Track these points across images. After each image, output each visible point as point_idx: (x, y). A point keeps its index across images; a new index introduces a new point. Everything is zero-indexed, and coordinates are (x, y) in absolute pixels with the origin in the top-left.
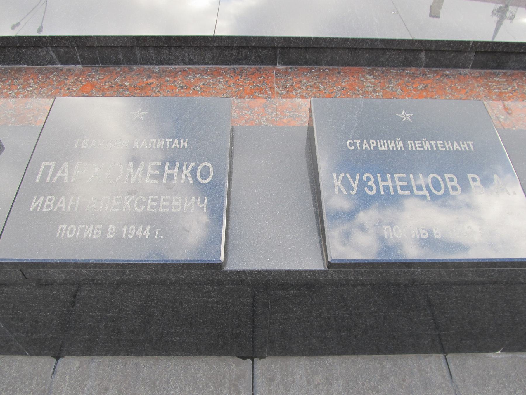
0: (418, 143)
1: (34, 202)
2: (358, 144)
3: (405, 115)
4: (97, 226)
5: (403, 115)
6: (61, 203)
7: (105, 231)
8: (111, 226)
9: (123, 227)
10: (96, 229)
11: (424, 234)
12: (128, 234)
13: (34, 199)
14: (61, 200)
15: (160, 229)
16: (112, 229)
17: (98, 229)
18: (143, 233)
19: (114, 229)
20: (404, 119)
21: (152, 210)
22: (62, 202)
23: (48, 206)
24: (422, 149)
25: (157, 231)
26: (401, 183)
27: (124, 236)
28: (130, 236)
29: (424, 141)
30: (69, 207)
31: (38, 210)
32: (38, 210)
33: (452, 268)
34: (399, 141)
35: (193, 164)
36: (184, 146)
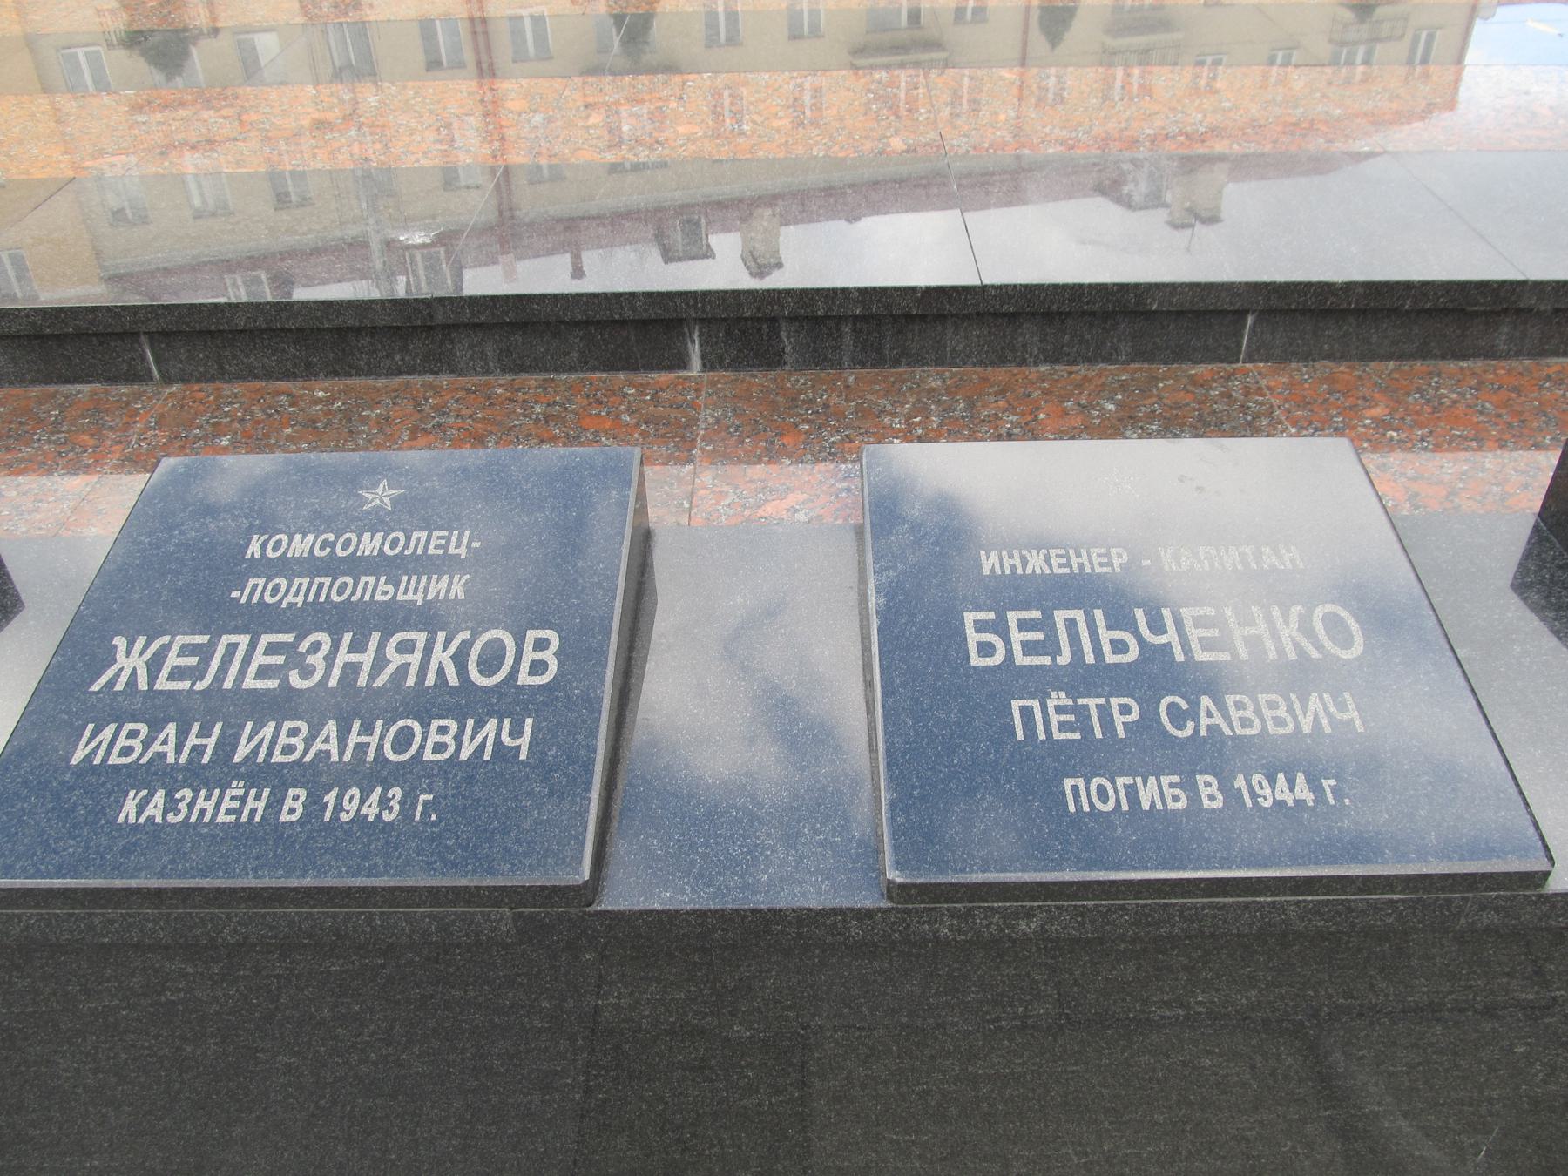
3: (382, 501)
6: (1210, 715)
7: (275, 804)
8: (292, 792)
9: (327, 792)
11: (1176, 799)
12: (338, 808)
13: (87, 734)
19: (303, 798)
20: (381, 487)
22: (328, 738)
23: (289, 749)
24: (1067, 571)
26: (1062, 718)
27: (328, 816)
33: (993, 902)
35: (466, 635)
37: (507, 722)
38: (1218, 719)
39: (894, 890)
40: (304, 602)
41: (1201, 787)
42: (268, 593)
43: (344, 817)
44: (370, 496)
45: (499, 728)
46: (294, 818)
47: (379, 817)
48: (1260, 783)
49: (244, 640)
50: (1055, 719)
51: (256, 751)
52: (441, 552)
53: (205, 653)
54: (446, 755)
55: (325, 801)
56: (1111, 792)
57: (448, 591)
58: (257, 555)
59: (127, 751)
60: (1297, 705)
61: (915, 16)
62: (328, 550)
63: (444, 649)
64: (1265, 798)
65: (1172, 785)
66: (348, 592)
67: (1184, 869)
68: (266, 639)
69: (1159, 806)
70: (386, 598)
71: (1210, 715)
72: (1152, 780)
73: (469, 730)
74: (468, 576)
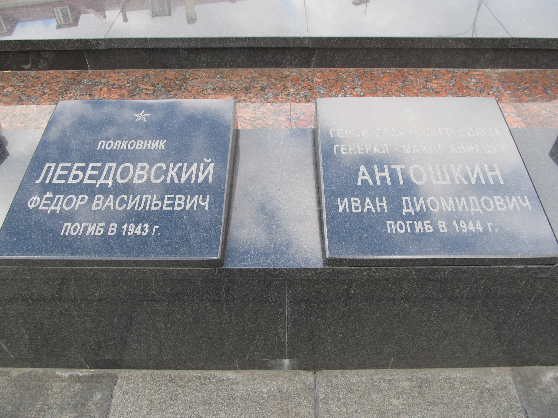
3: (142, 118)
5: (144, 116)
9: (124, 224)
10: (98, 227)
11: (429, 229)
12: (127, 231)
13: (195, 206)
14: (109, 199)
15: (157, 227)
16: (113, 227)
21: (168, 209)
25: (154, 230)
27: (124, 234)
28: (129, 234)
29: (205, 163)
36: (147, 146)
37: (201, 196)
38: (371, 206)
41: (440, 225)
42: (107, 146)
43: (129, 234)
44: (138, 116)
45: (198, 198)
46: (113, 234)
47: (141, 234)
48: (132, 227)
49: (53, 165)
51: (134, 206)
53: (101, 169)
54: (182, 207)
56: (398, 228)
57: (151, 144)
58: (125, 148)
60: (508, 200)
63: (173, 170)
64: (464, 229)
65: (427, 224)
66: (112, 146)
68: (61, 165)
69: (422, 231)
70: (140, 148)
71: (364, 175)
72: (420, 222)
73: (189, 199)
74: (165, 141)
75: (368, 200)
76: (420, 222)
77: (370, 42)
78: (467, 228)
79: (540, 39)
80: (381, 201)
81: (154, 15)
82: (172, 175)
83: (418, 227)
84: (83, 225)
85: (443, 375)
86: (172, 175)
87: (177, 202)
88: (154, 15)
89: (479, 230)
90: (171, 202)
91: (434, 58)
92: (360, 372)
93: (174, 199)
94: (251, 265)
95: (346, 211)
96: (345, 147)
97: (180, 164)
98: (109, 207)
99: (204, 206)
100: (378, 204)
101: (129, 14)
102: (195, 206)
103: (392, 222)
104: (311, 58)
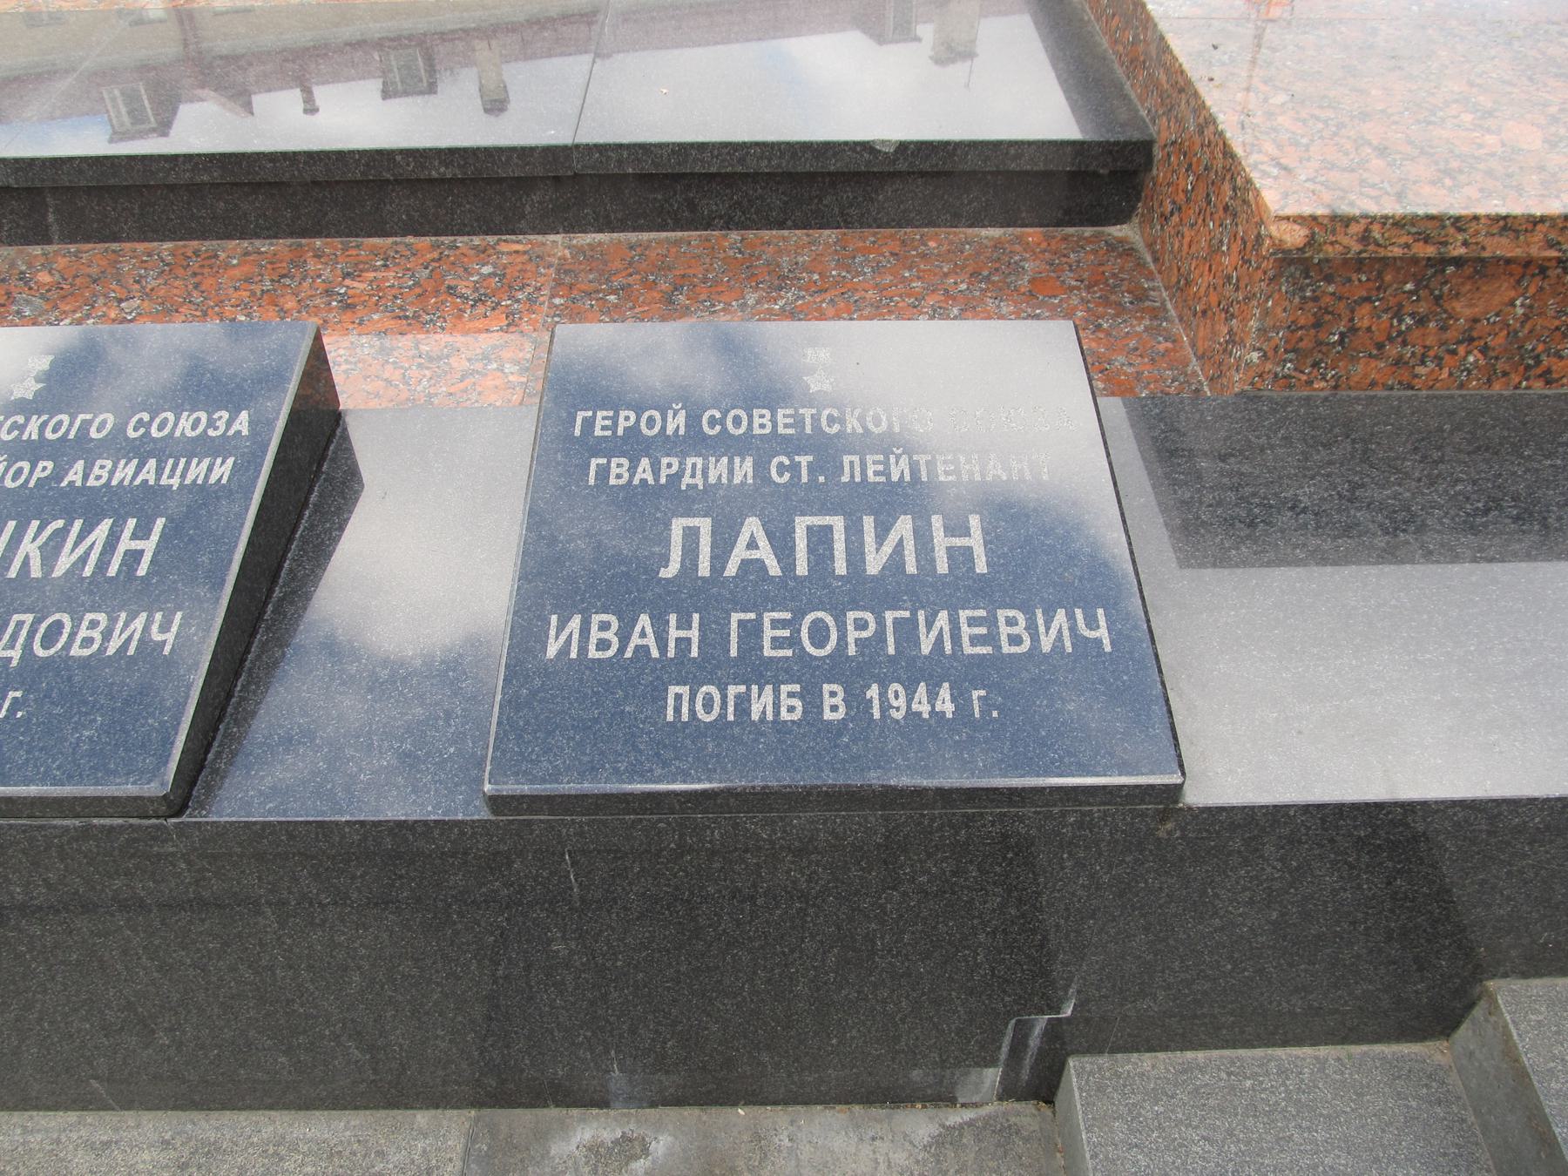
0: (874, 463)
1: (552, 632)
2: (808, 421)
4: (785, 689)
6: (643, 634)
7: (811, 699)
8: (826, 688)
11: (791, 709)
13: (134, 644)
17: (791, 695)
18: (933, 706)
23: (603, 645)
24: (883, 479)
30: (672, 644)
31: (573, 655)
32: (573, 655)
34: (901, 455)
38: (650, 641)
39: (496, 802)
40: (181, 484)
41: (826, 696)
50: (966, 631)
52: (608, 433)
54: (610, 653)
55: (868, 697)
59: (88, 642)
60: (1040, 621)
61: (185, 18)
62: (718, 428)
63: (34, 540)
67: (1047, 774)
69: (770, 717)
71: (643, 634)
72: (769, 689)
75: (644, 620)
76: (769, 689)
77: (172, 169)
78: (909, 707)
79: (661, 146)
80: (684, 624)
81: (387, 94)
82: (27, 557)
83: (762, 703)
84: (733, 690)
85: (267, 1132)
86: (27, 557)
87: (1004, 630)
88: (387, 94)
89: (944, 713)
90: (786, 633)
91: (388, 207)
92: (36, 1119)
93: (991, 621)
94: (270, 812)
95: (568, 653)
96: (879, 463)
97: (60, 523)
98: (642, 650)
99: (1099, 642)
100: (674, 633)
101: (321, 93)
102: (134, 644)
103: (684, 690)
104: (44, 216)
